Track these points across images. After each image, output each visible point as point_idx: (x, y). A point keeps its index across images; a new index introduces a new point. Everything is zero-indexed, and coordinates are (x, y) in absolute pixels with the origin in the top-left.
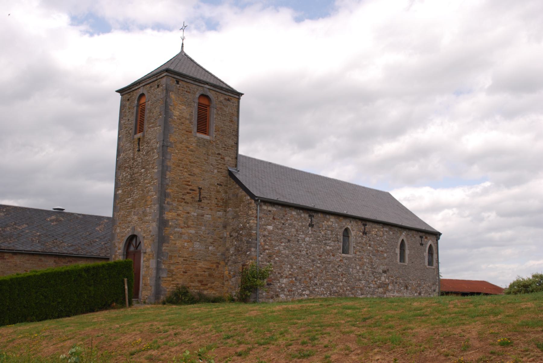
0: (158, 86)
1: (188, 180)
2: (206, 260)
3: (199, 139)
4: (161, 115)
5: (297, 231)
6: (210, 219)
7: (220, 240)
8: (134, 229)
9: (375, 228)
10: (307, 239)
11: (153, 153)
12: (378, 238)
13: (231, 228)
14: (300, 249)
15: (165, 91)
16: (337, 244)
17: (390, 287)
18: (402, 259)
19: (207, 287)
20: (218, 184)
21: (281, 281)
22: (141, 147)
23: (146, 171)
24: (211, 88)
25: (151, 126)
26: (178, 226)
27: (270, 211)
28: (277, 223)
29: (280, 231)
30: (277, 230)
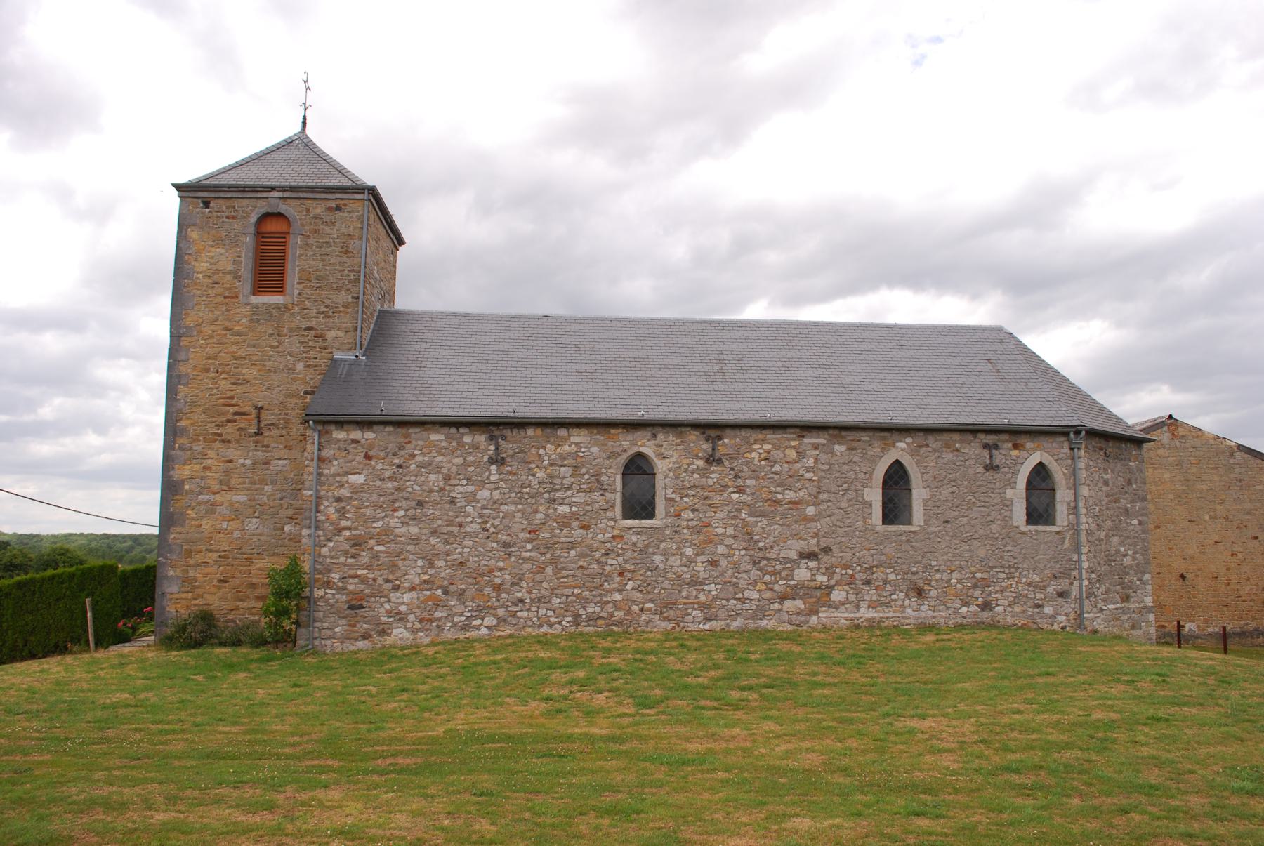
1: (229, 394)
2: (274, 554)
3: (256, 306)
5: (447, 478)
6: (288, 468)
9: (764, 441)
10: (484, 494)
17: (837, 596)
21: (393, 599)
24: (287, 194)
26: (205, 489)
27: (354, 441)
28: (380, 466)
30: (379, 483)
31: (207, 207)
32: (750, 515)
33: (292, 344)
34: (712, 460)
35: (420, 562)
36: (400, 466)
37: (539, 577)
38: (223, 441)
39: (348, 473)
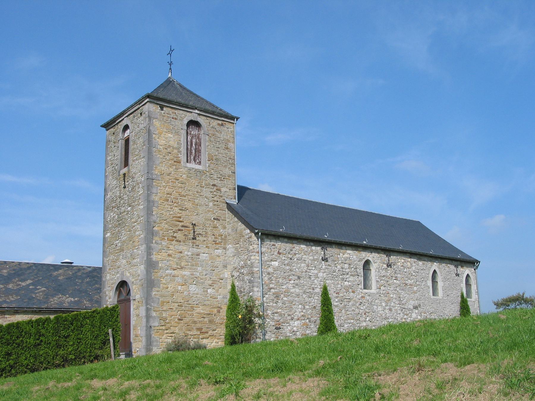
0: (141, 114)
1: (179, 215)
4: (144, 145)
5: (308, 266)
7: (221, 281)
8: (122, 274)
11: (139, 188)
12: (405, 270)
13: (232, 267)
14: (313, 286)
15: (147, 119)
16: (357, 279)
18: (435, 293)
19: (207, 335)
20: (214, 219)
22: (126, 183)
23: (132, 209)
25: (135, 158)
28: (283, 258)
29: (288, 268)
30: (283, 266)
31: (162, 110)
32: (400, 290)
33: (206, 192)
34: (389, 265)
35: (300, 306)
36: (291, 259)
37: (340, 315)
38: (177, 241)
39: (271, 260)
